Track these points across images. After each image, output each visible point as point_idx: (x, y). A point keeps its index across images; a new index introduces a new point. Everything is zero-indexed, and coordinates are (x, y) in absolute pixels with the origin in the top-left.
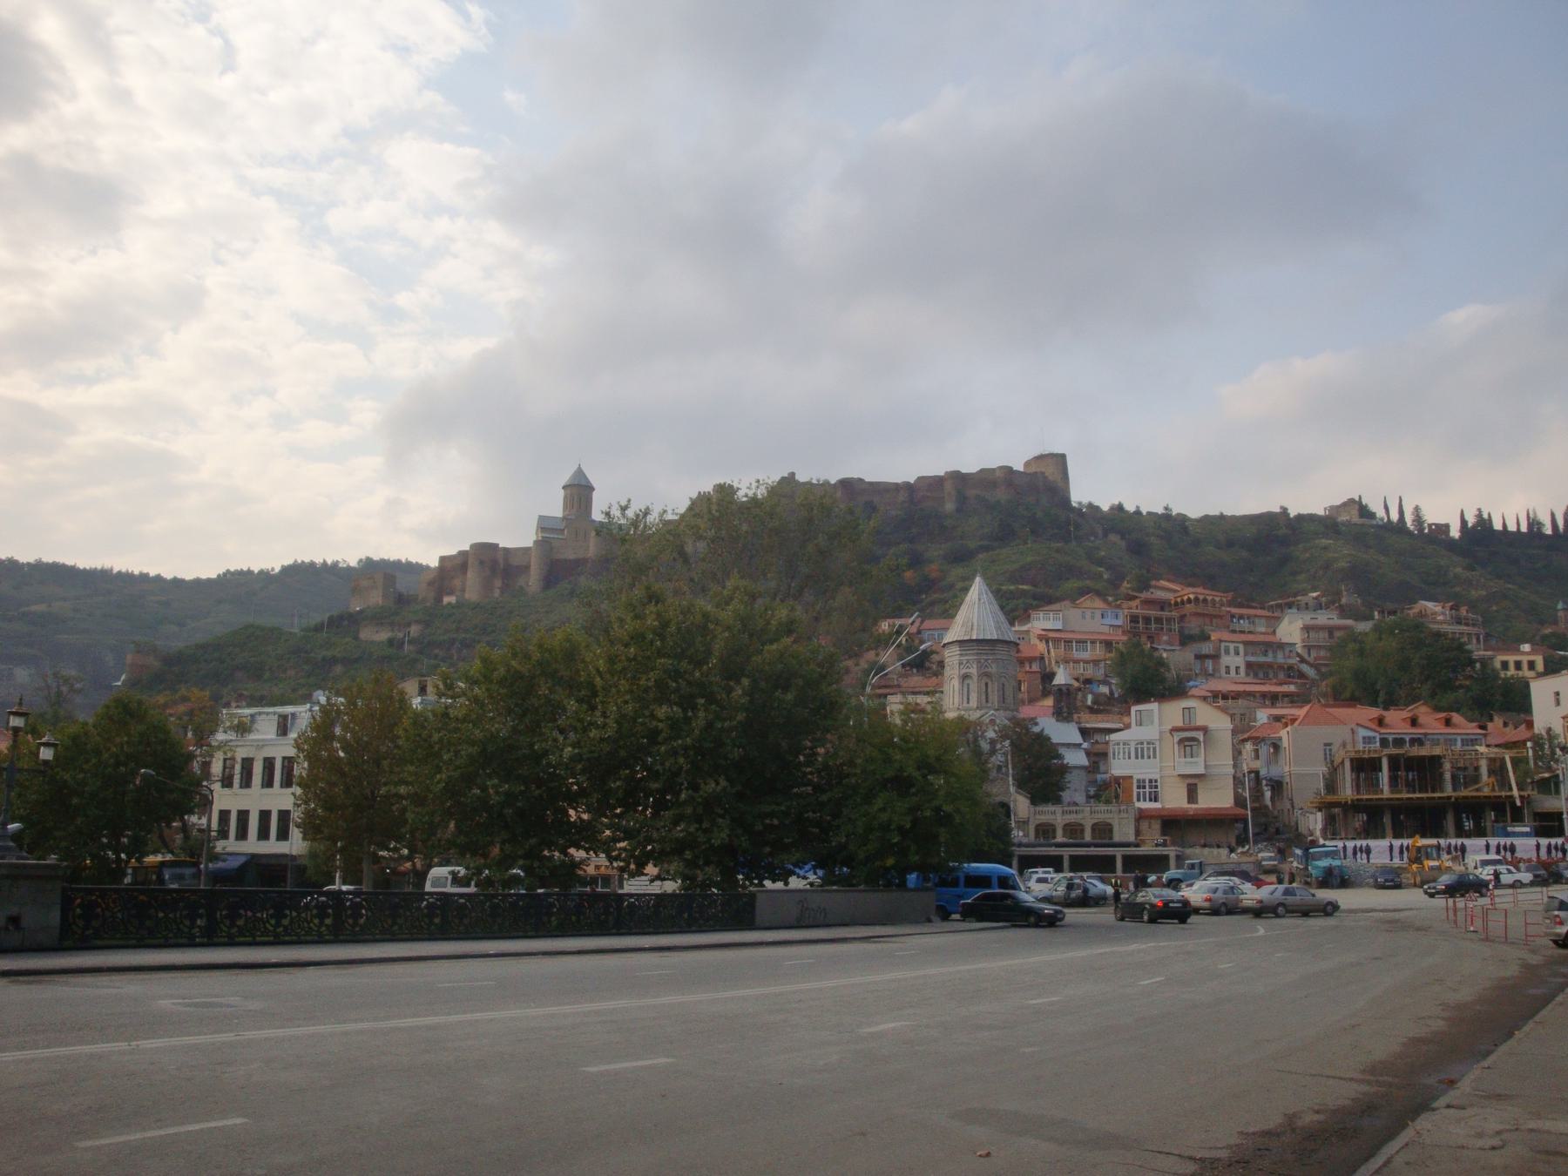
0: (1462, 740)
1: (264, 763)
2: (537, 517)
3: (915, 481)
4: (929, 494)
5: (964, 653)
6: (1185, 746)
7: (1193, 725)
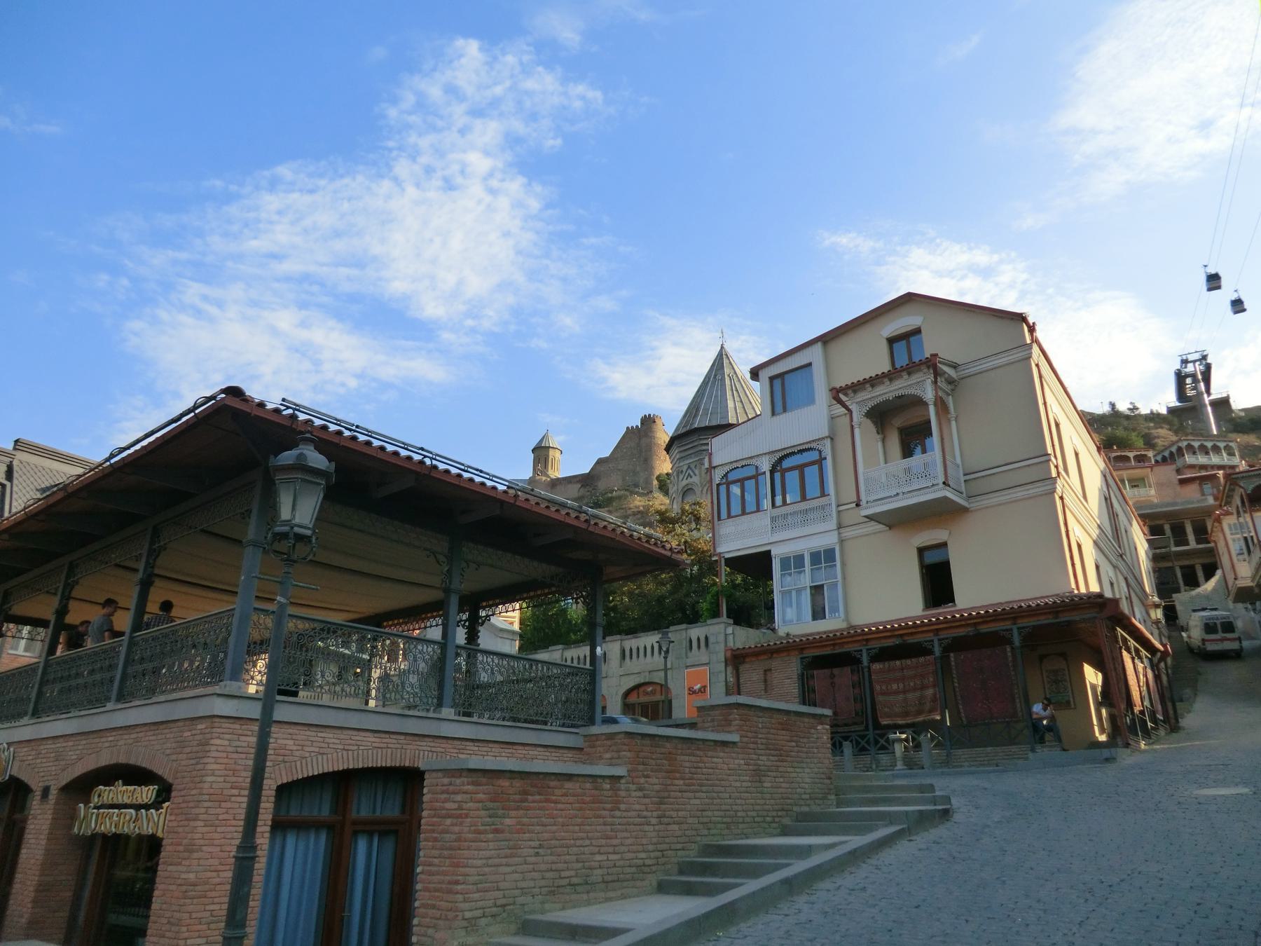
5: (683, 455)
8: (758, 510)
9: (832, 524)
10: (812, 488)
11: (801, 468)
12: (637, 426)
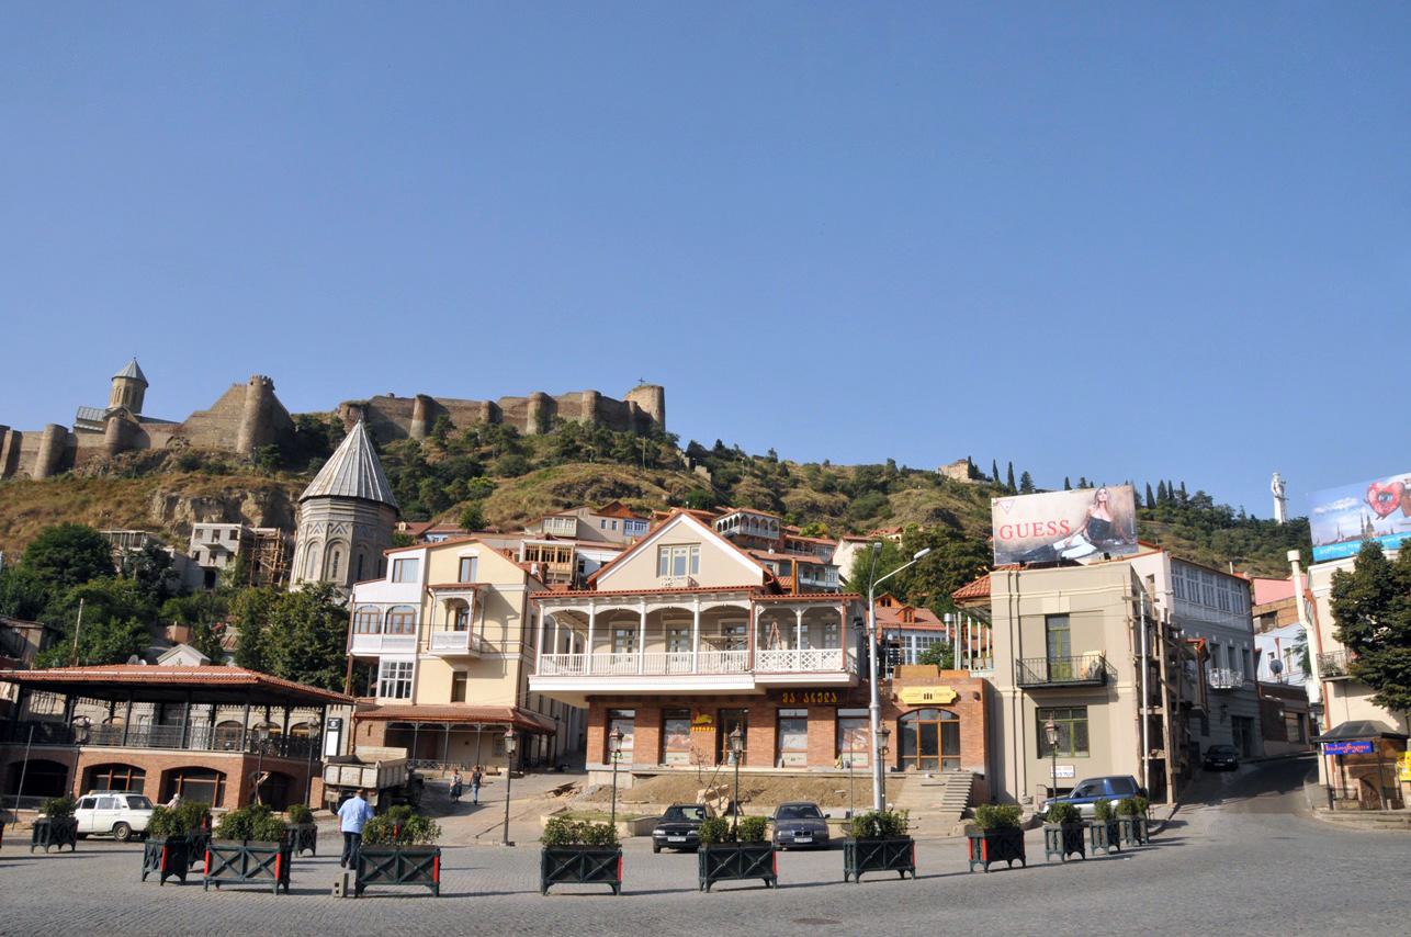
0: (918, 639)
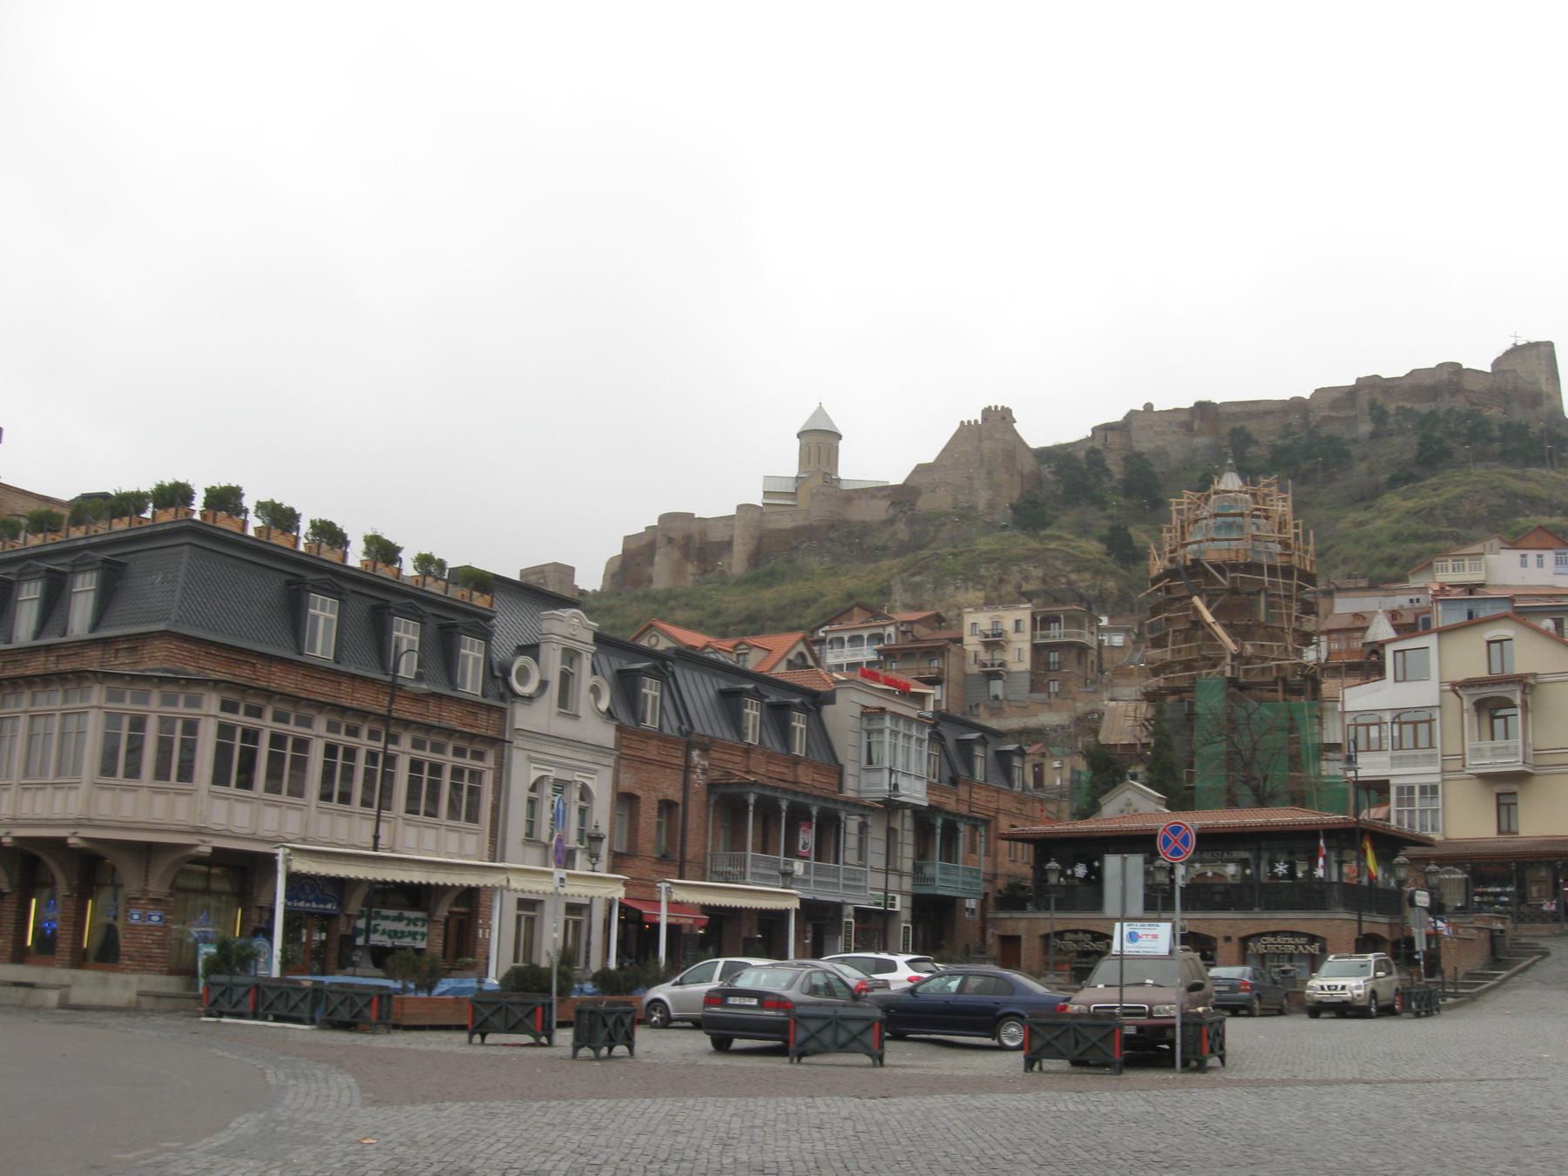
1: (477, 815)
2: (762, 479)
3: (1312, 396)
4: (1334, 414)
6: (1493, 717)
7: (1508, 672)
8: (1380, 749)
9: (1437, 769)
10: (1423, 742)
11: (1415, 723)
12: (976, 421)
